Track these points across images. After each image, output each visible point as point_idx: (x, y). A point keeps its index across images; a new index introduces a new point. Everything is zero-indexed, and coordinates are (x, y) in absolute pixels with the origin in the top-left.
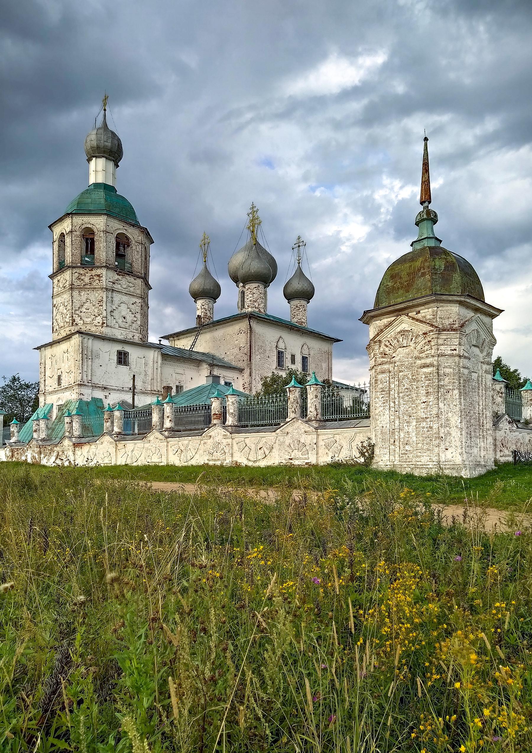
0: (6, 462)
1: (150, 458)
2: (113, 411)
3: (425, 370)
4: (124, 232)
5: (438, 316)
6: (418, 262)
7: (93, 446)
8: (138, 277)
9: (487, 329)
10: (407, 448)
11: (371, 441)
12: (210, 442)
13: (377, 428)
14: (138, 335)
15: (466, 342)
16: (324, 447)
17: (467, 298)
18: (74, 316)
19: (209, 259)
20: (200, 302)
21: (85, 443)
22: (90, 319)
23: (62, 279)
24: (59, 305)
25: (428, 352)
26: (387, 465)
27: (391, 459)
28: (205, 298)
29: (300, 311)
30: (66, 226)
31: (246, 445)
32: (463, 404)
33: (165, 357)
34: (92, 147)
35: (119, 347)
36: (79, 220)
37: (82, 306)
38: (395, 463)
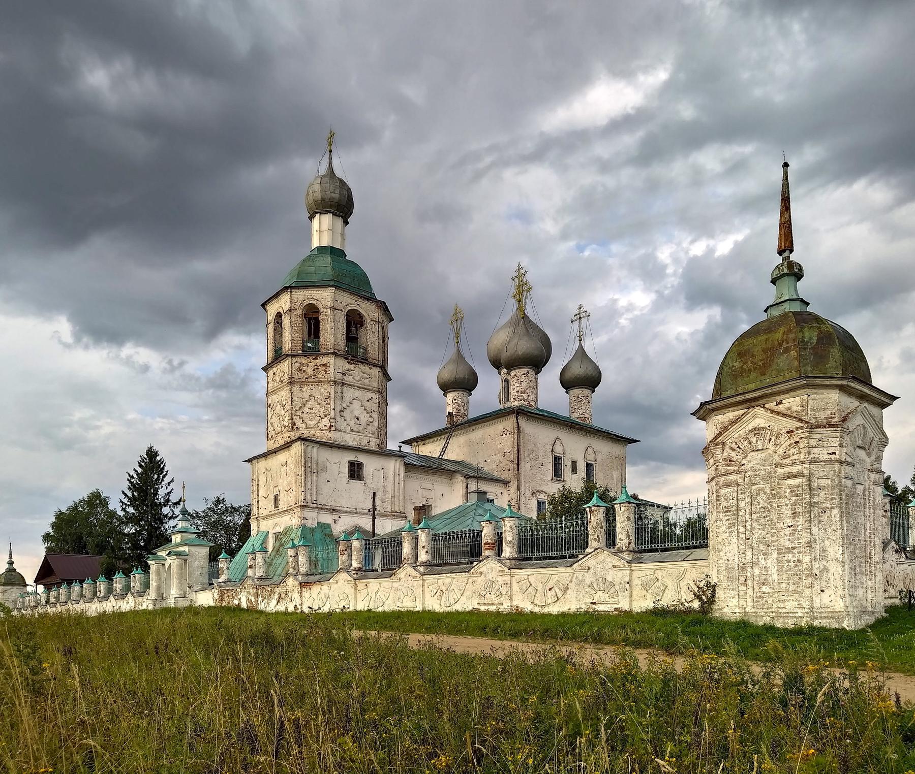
0: (214, 607)
2: (350, 541)
3: (790, 482)
5: (809, 408)
6: (778, 333)
7: (325, 587)
8: (374, 366)
9: (877, 424)
10: (764, 588)
11: (710, 580)
12: (480, 580)
13: (720, 562)
14: (375, 440)
15: (849, 442)
16: (641, 587)
17: (851, 382)
18: (294, 417)
19: (462, 339)
20: (451, 396)
25: (795, 457)
26: (735, 613)
27: (741, 604)
28: (458, 391)
29: (582, 403)
30: (283, 303)
31: (531, 585)
32: (845, 529)
33: (409, 467)
34: (315, 201)
35: (351, 457)
36: (301, 295)
37: (305, 404)
38: (747, 610)
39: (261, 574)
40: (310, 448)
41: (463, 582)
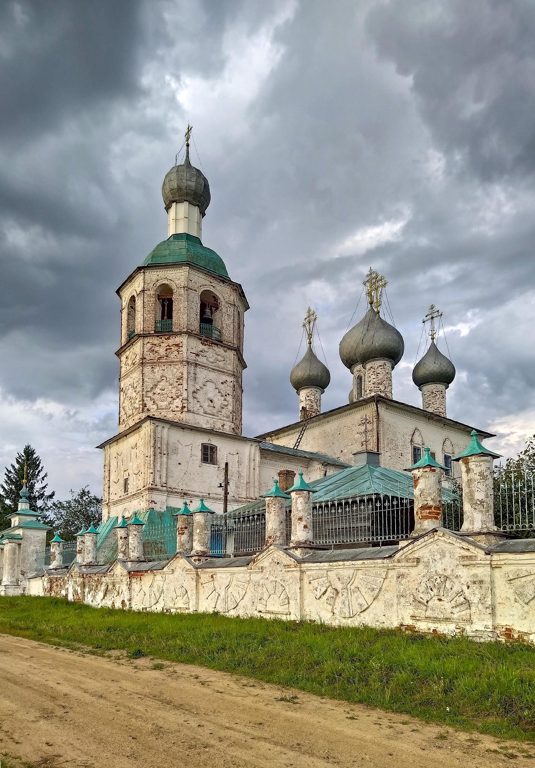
0: (43, 598)
1: (264, 603)
4: (211, 290)
7: (158, 577)
14: (229, 424)
18: (145, 399)
20: (303, 393)
21: (146, 571)
22: (166, 403)
23: (131, 353)
24: (128, 388)
29: (436, 398)
35: (205, 439)
36: (153, 276)
37: (156, 385)
39: (90, 560)
40: (159, 428)
41: (377, 575)
